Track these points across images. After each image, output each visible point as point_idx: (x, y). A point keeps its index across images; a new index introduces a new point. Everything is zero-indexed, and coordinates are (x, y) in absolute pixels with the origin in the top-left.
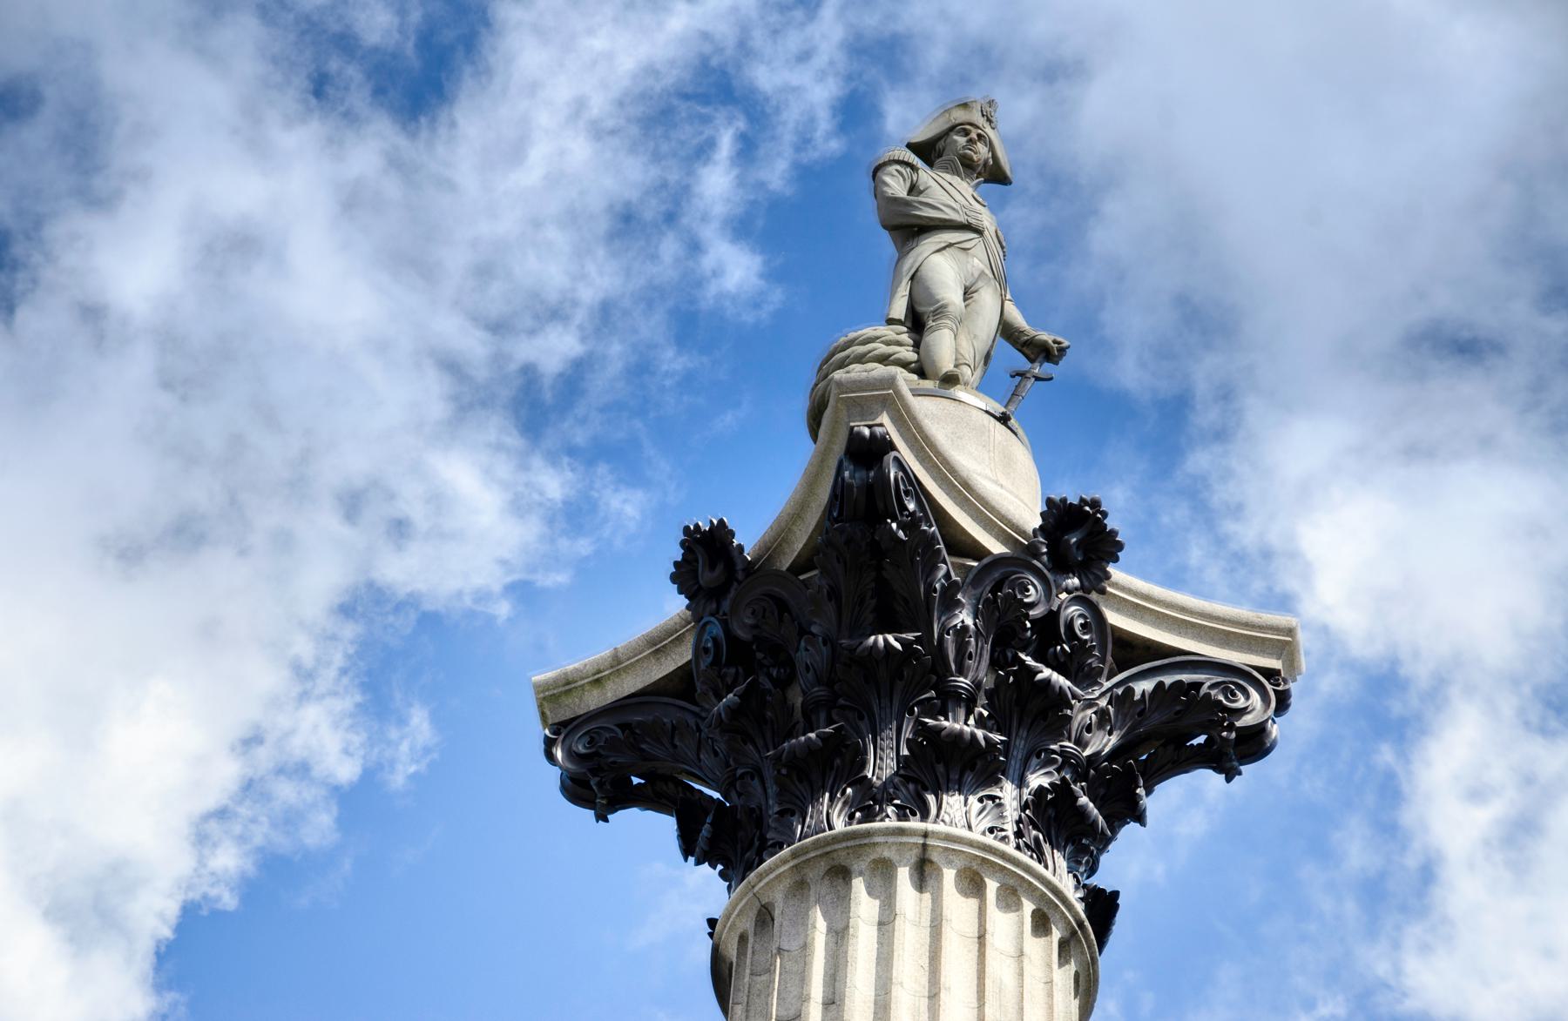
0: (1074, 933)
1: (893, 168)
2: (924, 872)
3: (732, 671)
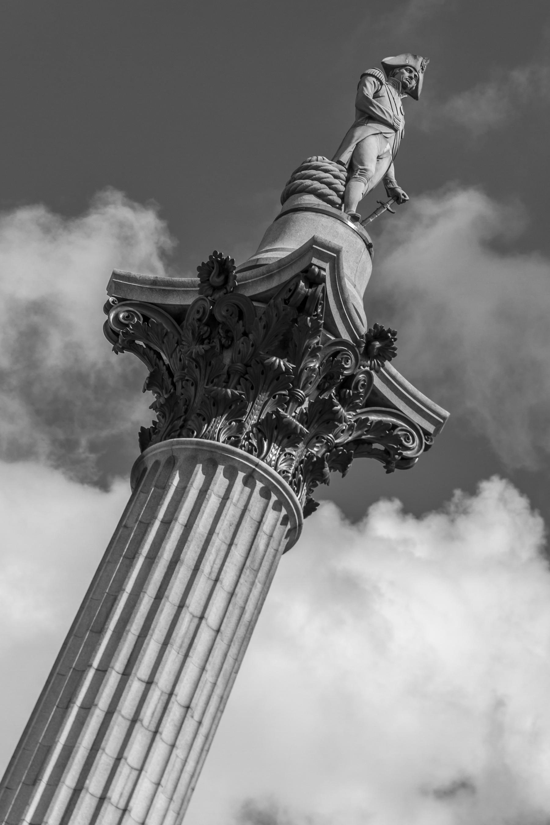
0: (296, 528)
1: (372, 79)
2: (249, 481)
3: (206, 328)
